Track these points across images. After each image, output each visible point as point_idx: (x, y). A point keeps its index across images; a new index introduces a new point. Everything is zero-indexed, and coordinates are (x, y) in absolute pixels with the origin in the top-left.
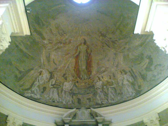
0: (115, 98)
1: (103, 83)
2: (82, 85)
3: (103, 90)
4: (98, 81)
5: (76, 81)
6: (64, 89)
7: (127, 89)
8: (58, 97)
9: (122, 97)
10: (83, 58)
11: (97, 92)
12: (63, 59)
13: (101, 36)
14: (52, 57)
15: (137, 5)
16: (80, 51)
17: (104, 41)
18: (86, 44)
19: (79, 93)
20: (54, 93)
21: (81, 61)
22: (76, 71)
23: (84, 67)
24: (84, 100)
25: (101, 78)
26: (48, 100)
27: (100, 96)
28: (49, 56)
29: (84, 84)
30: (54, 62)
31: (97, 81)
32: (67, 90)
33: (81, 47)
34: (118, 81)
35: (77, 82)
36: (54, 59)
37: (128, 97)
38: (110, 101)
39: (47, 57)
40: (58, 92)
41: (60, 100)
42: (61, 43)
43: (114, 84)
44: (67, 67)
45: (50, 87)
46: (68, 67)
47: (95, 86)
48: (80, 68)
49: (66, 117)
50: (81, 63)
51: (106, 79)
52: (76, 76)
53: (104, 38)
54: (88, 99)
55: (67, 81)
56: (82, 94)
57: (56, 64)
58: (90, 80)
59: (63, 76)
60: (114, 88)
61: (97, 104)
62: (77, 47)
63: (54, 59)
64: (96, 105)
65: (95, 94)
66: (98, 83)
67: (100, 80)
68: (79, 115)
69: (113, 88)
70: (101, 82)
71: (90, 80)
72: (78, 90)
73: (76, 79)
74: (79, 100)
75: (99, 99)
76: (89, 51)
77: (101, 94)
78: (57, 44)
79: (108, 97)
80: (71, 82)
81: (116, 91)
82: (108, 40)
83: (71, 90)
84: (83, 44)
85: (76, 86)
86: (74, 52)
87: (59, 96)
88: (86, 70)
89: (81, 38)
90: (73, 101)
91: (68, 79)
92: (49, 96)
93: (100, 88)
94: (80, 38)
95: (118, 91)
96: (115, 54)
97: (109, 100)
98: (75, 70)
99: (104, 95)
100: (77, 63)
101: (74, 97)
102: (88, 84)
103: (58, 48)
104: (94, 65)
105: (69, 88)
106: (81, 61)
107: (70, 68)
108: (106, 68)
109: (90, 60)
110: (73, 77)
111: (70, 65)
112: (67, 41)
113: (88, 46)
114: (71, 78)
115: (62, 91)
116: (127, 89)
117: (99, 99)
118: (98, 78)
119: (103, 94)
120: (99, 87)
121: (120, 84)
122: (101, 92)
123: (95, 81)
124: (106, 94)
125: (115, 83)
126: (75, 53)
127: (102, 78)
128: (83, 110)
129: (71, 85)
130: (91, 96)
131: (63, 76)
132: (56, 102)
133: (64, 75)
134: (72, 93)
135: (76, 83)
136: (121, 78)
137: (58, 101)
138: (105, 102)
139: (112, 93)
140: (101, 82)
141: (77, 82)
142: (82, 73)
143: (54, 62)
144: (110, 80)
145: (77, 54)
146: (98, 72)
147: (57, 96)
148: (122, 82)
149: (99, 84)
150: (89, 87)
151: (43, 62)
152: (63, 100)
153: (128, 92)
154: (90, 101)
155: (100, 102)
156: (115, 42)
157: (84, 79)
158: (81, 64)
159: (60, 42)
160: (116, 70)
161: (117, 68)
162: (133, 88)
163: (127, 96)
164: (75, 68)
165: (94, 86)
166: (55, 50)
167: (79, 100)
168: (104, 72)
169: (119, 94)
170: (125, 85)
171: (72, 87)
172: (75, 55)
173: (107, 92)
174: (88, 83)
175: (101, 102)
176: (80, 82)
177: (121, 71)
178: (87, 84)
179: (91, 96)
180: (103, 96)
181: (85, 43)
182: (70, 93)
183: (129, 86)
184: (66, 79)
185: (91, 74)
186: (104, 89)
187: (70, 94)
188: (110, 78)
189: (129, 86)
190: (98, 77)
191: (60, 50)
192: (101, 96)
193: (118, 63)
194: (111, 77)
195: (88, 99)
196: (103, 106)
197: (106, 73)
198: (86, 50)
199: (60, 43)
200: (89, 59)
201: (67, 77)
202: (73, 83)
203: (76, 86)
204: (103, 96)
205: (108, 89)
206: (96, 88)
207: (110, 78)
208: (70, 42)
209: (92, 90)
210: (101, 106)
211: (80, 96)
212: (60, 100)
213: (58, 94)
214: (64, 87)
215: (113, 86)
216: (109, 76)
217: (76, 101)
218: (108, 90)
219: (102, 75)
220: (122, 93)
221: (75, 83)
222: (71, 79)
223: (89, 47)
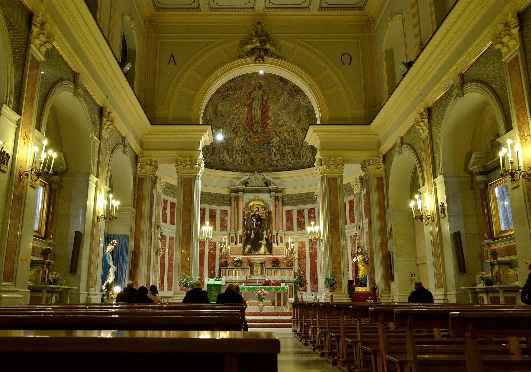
0: (292, 161)
1: (280, 139)
2: (255, 140)
3: (279, 149)
4: (275, 136)
5: (248, 136)
6: (235, 147)
7: (306, 153)
8: (229, 158)
9: (299, 161)
10: (257, 104)
11: (272, 150)
12: (232, 109)
13: (282, 81)
14: (220, 108)
15: (208, 339)
16: (254, 98)
17: (285, 88)
18: (262, 89)
19: (252, 151)
20: (224, 154)
21: (254, 110)
22: (248, 123)
23: (258, 118)
24: (258, 161)
25: (279, 134)
26: (219, 162)
27: (275, 157)
28: (216, 109)
29: (257, 140)
30: (222, 115)
31: (274, 137)
32: (237, 148)
33: (255, 92)
34: (297, 141)
35: (250, 137)
36: (221, 111)
37: (305, 163)
38: (286, 164)
39: (213, 110)
40: (228, 150)
41: (231, 161)
42: (230, 91)
43: (293, 143)
44: (237, 118)
45: (220, 146)
46: (239, 118)
47: (271, 143)
48: (253, 119)
49: (239, 185)
50: (254, 111)
51: (285, 135)
52: (248, 129)
53: (285, 84)
54: (261, 159)
55: (237, 137)
56: (255, 153)
57: (224, 117)
58: (265, 135)
59: (233, 131)
60: (292, 148)
61: (272, 166)
62: (251, 93)
63: (221, 111)
64: (270, 167)
65: (270, 153)
66: (274, 139)
67: (277, 136)
68: (252, 180)
69: (291, 147)
70: (278, 139)
71: (265, 135)
72: (251, 147)
73: (249, 134)
74: (252, 159)
75: (274, 159)
76: (265, 98)
77: (277, 153)
78: (225, 92)
79: (284, 158)
80: (242, 138)
81: (293, 152)
82: (289, 88)
83: (242, 148)
84: (257, 89)
85: (248, 143)
86: (246, 99)
87: (229, 156)
88: (260, 122)
89: (255, 82)
90: (246, 161)
91: (238, 134)
92: (219, 158)
93: (276, 146)
94: (254, 82)
95: (296, 154)
96: (297, 106)
97: (285, 162)
98: (248, 121)
99: (280, 155)
100: (249, 111)
101: (247, 156)
102: (263, 140)
103: (226, 97)
104: (271, 116)
105: (241, 146)
106: (254, 110)
107: (241, 118)
108: (285, 121)
109: (266, 109)
110: (245, 130)
111: (241, 115)
112: (237, 87)
113: (264, 91)
114: (242, 132)
115: (232, 150)
116: (306, 153)
117: (274, 159)
118: (274, 133)
119: (279, 154)
120: (276, 145)
121: (300, 144)
122: (277, 151)
123: (272, 137)
124: (283, 155)
125: (294, 142)
126: (247, 101)
127: (280, 133)
128: (256, 174)
129: (243, 141)
130: (266, 154)
131: (233, 131)
132: (227, 163)
133: (234, 128)
134: (244, 151)
135: (249, 138)
136: (301, 137)
137: (229, 162)
138: (281, 164)
139: (289, 154)
140: (278, 139)
141: (250, 137)
142: (256, 126)
143: (222, 115)
144: (288, 138)
145: (249, 101)
146: (276, 125)
147: (228, 156)
148: (302, 142)
149: (276, 141)
150: (264, 144)
151: (210, 117)
152: (234, 161)
153: (307, 157)
154: (264, 162)
155: (275, 163)
156: (299, 91)
157: (258, 134)
158: (255, 114)
159: (229, 89)
160: (297, 127)
161: (298, 124)
162: (312, 153)
163: (304, 161)
164: (247, 119)
165: (269, 142)
166: (223, 99)
167: (252, 159)
168: (283, 126)
169: (297, 156)
170: (304, 147)
171: (243, 143)
172: (248, 103)
173: (284, 152)
174: (263, 138)
175: (277, 164)
176: (253, 137)
177: (302, 128)
178: (261, 140)
179: (266, 154)
180: (279, 156)
181: (260, 88)
182: (241, 151)
183: (308, 149)
184: (237, 134)
185: (266, 126)
186: (281, 147)
187: (242, 152)
188: (289, 135)
189: (308, 149)
190: (275, 131)
191: (228, 99)
192: (277, 156)
193: (300, 118)
194: (290, 133)
195: (261, 159)
196: (278, 168)
197: (284, 128)
198: (262, 96)
199: (229, 90)
200: (264, 109)
201: (237, 131)
202: (245, 138)
203: (248, 143)
204: (279, 156)
205: (285, 148)
206: (271, 145)
207: (289, 135)
208: (241, 88)
209: (267, 147)
210: (277, 169)
211: (253, 155)
212: (231, 161)
213: (228, 154)
214: (234, 145)
215: (291, 146)
216: (287, 132)
217: (249, 161)
218: (285, 150)
219: (280, 129)
220: (300, 157)
221: (247, 139)
222: (242, 133)
223: (265, 93)
